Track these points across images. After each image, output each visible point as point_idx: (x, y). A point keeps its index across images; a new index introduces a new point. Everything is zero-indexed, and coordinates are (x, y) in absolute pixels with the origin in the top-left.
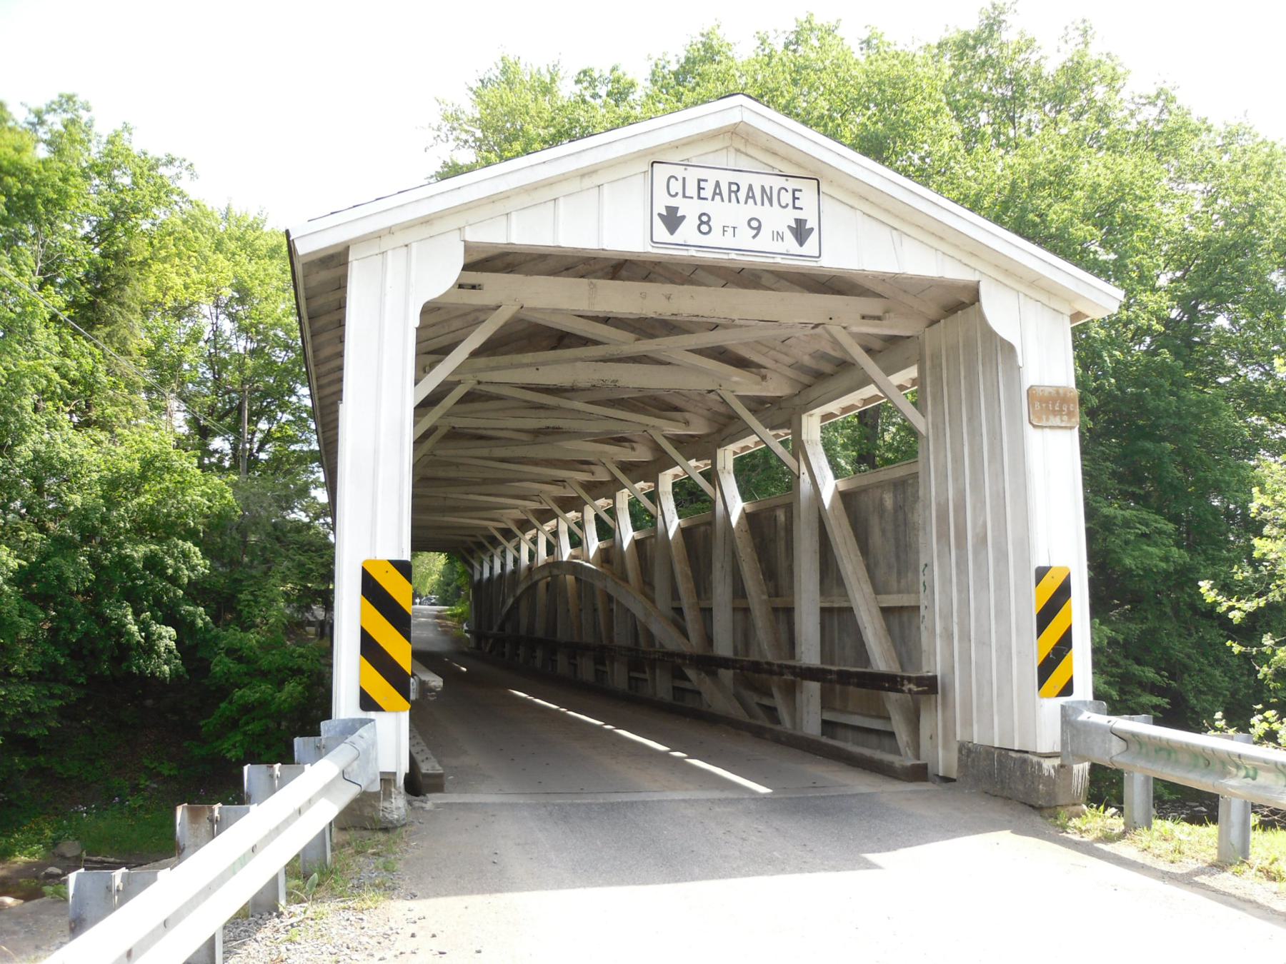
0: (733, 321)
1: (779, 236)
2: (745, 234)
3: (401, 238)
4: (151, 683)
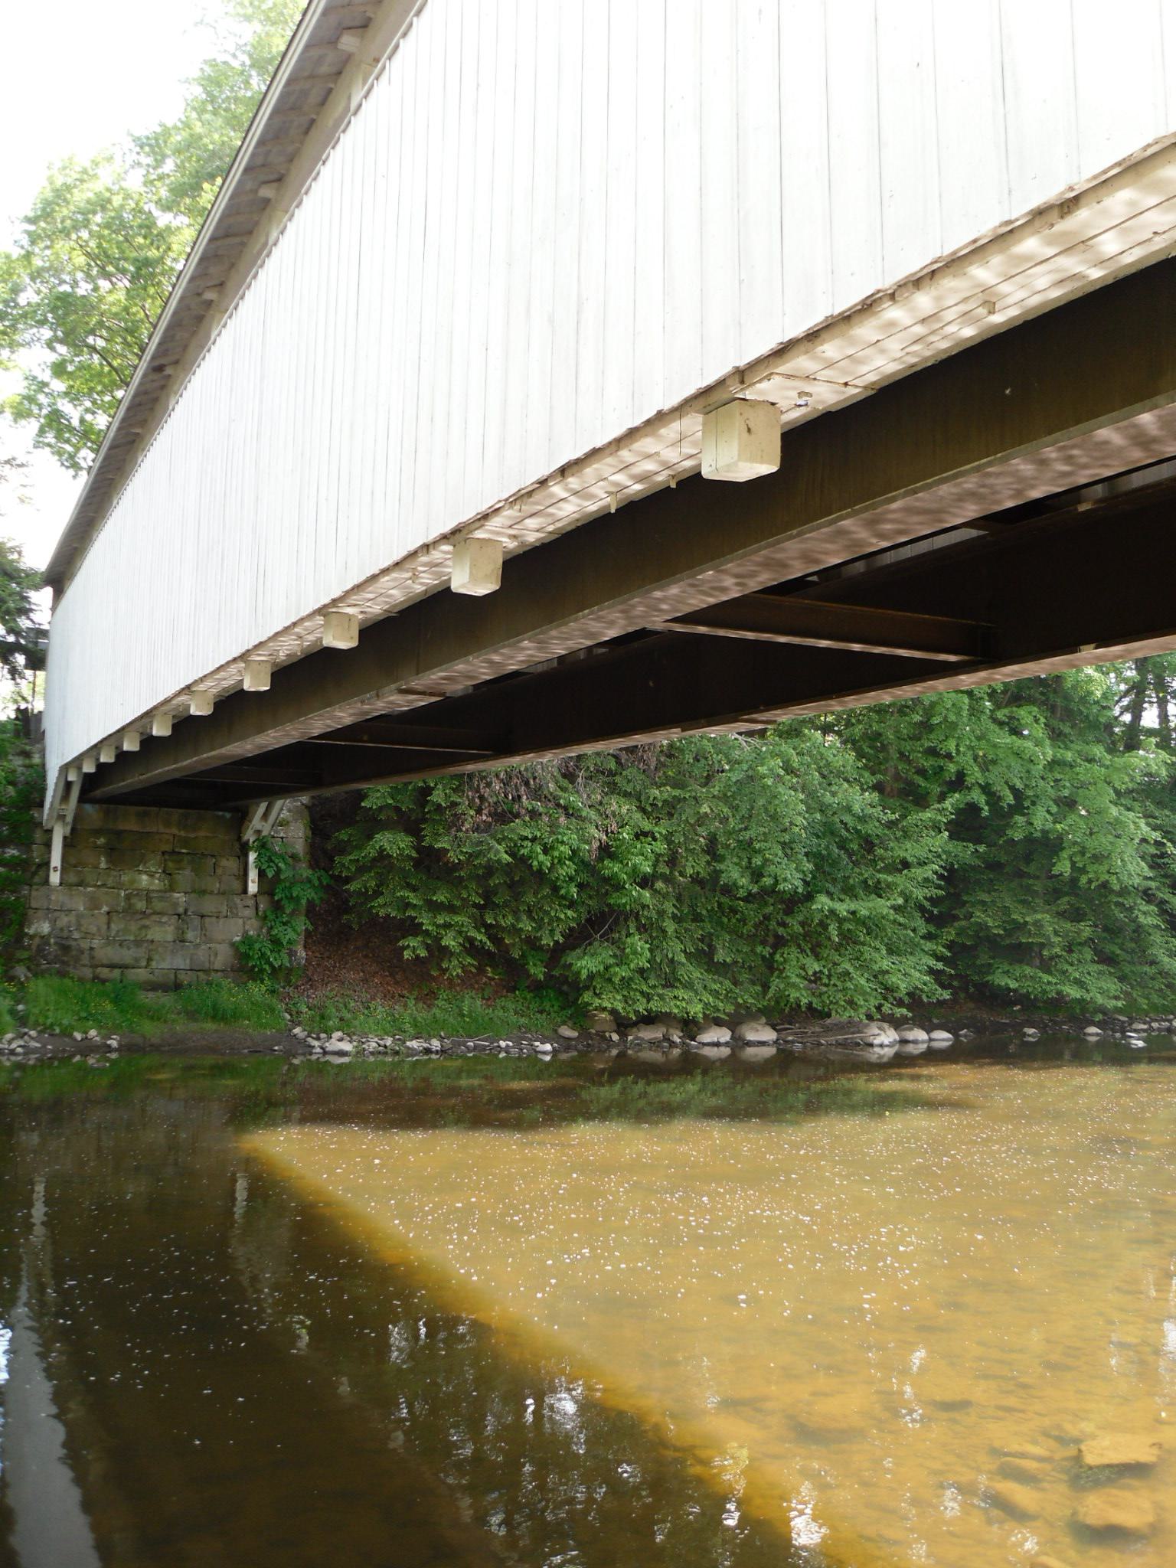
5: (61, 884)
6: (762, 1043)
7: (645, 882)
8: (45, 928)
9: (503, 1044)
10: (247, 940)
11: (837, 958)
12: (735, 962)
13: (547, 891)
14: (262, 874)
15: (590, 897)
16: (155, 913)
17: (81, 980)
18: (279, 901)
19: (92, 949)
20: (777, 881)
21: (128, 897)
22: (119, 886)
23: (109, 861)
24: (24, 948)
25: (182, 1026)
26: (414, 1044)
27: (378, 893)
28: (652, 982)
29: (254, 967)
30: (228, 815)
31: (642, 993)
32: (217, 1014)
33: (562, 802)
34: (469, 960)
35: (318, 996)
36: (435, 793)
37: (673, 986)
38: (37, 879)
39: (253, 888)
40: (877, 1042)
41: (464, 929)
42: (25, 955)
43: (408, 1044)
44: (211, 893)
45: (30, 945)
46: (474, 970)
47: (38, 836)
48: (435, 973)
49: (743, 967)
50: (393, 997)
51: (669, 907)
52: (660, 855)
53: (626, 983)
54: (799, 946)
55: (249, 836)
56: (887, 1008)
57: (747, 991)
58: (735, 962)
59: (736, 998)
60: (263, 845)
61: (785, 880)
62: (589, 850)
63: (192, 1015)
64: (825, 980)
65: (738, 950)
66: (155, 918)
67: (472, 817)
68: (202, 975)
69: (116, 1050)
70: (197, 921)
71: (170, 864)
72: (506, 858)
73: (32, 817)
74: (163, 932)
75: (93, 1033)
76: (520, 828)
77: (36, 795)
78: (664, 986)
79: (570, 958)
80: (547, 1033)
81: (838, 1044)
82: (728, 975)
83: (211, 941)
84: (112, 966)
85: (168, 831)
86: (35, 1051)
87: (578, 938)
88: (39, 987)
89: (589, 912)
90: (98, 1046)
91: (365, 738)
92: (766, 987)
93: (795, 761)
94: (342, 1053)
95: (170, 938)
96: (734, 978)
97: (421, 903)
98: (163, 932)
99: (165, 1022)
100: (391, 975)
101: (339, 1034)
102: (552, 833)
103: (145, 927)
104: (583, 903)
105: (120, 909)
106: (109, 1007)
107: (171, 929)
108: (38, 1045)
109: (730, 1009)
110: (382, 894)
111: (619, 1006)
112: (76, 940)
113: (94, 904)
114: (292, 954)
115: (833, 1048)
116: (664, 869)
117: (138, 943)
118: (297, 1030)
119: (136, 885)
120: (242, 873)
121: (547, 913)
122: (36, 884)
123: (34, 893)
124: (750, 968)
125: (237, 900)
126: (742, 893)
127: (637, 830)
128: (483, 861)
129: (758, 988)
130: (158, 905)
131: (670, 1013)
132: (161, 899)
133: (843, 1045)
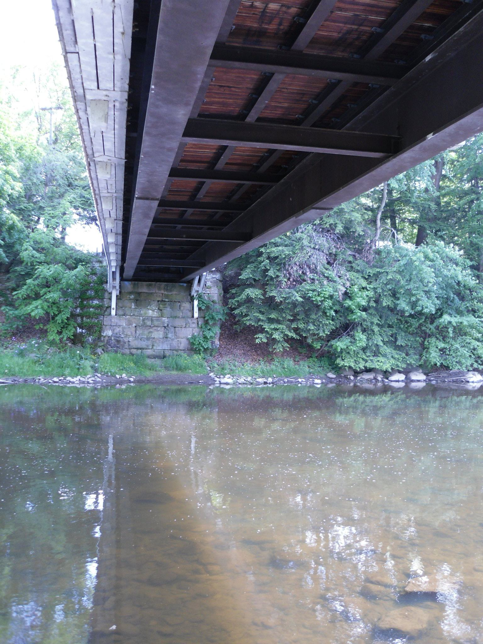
5: (116, 315)
6: (419, 381)
7: (365, 309)
8: (110, 333)
9: (300, 380)
10: (194, 337)
11: (453, 342)
12: (407, 345)
13: (321, 313)
14: (200, 309)
15: (341, 316)
16: (154, 326)
17: (123, 354)
18: (207, 320)
19: (129, 341)
20: (423, 308)
21: (143, 320)
22: (140, 315)
23: (136, 305)
24: (101, 341)
25: (162, 373)
26: (260, 380)
27: (246, 315)
28: (368, 354)
29: (196, 348)
30: (185, 285)
31: (363, 359)
32: (179, 368)
33: (326, 275)
34: (286, 345)
35: (225, 360)
36: (269, 271)
37: (378, 356)
38: (106, 313)
39: (196, 315)
40: (471, 380)
41: (283, 331)
42: (102, 344)
43: (257, 380)
44: (179, 317)
45: (104, 340)
46: (288, 349)
47: (106, 295)
48: (271, 350)
49: (411, 347)
50: (256, 361)
51: (376, 321)
52: (371, 298)
53: (356, 354)
54: (436, 337)
55: (194, 293)
56: (475, 365)
57: (411, 358)
58: (407, 345)
59: (406, 361)
60: (200, 297)
61: (427, 308)
62: (339, 295)
63: (166, 368)
64: (448, 353)
65: (408, 340)
66: (155, 328)
67: (285, 282)
68: (175, 352)
69: (132, 382)
70: (172, 329)
71: (161, 306)
72: (300, 299)
73: (104, 287)
74: (158, 334)
75: (124, 375)
76: (306, 286)
77: (104, 278)
78: (374, 356)
79: (333, 342)
80: (322, 376)
81: (453, 381)
82: (405, 351)
83: (178, 337)
84: (137, 349)
85: (160, 292)
86: (99, 382)
87: (335, 334)
88: (105, 356)
89: (341, 323)
90: (125, 381)
91: (184, 236)
92: (421, 355)
93: (431, 255)
94: (227, 384)
95: (161, 336)
96: (407, 352)
97: (265, 319)
98: (158, 334)
99: (156, 371)
100: (256, 351)
101: (229, 376)
102: (321, 288)
103: (151, 332)
104: (338, 319)
105: (140, 325)
106: (132, 365)
107: (162, 333)
108: (101, 380)
109: (404, 366)
110: (249, 315)
111: (352, 365)
112: (122, 338)
113: (130, 323)
114: (213, 343)
115: (451, 383)
116: (373, 304)
117: (148, 339)
118: (212, 374)
119: (147, 315)
120: (191, 309)
121: (321, 322)
122: (106, 315)
123: (105, 319)
124: (414, 348)
125: (189, 320)
126: (407, 314)
127: (360, 287)
128: (289, 301)
129: (417, 357)
130: (156, 323)
131: (375, 368)
132: (157, 320)
133: (456, 382)
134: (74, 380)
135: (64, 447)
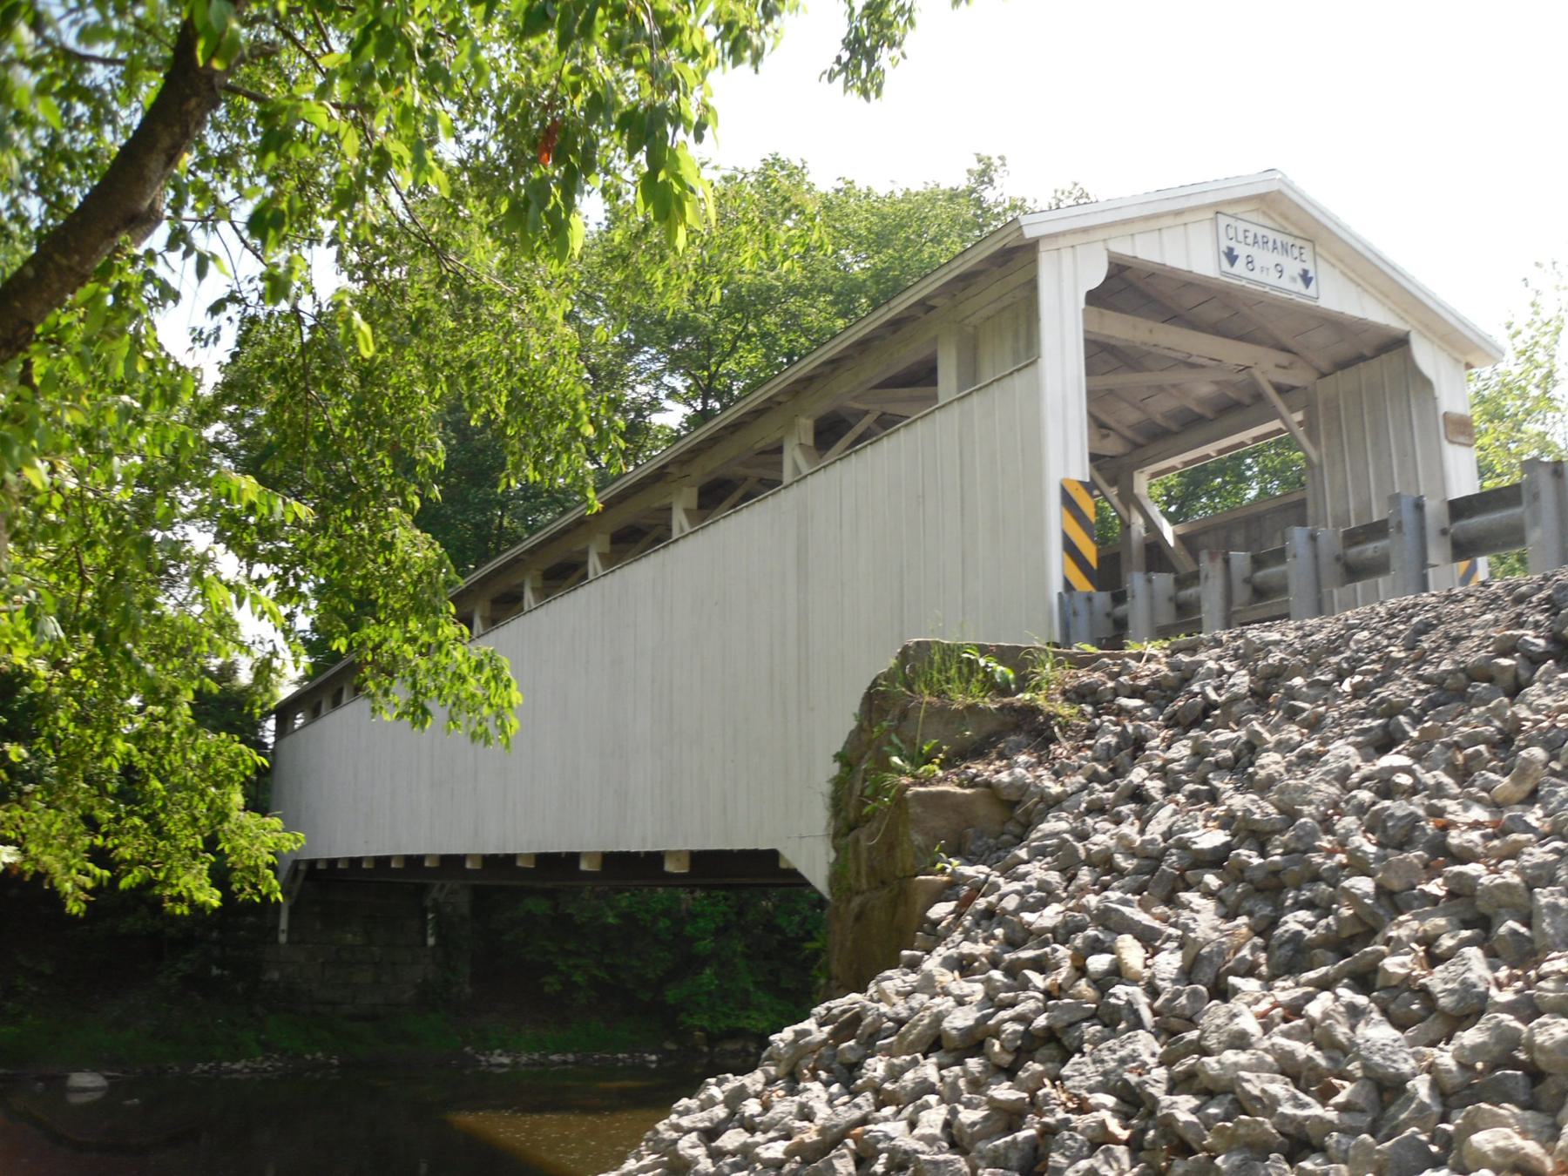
0: (1190, 356)
1: (1293, 279)
2: (1274, 274)
3: (1070, 240)
4: (1305, 415)
8: (276, 976)
26: (554, 1057)
134: (237, 1066)
135: (945, 753)
